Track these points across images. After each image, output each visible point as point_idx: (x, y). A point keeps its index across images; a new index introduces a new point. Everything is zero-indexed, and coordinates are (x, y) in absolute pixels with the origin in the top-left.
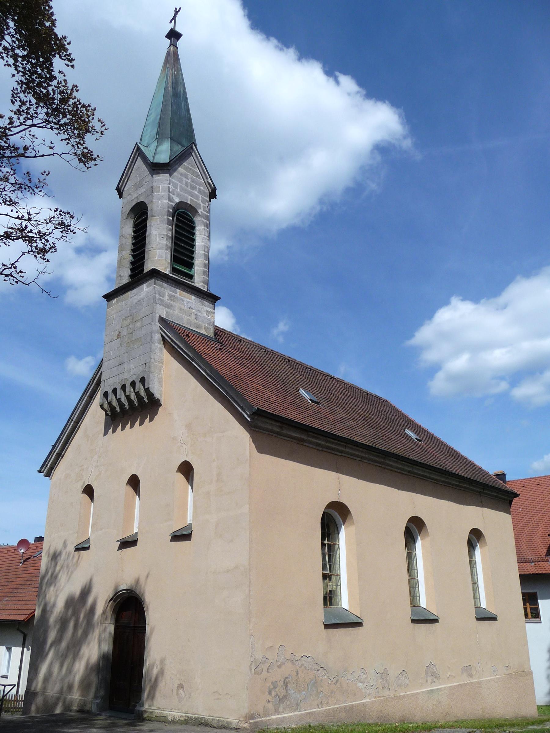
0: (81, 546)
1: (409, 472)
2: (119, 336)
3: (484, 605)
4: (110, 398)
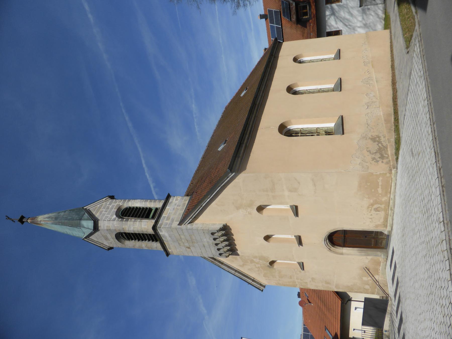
0: (302, 267)
1: (263, 93)
2: (189, 248)
3: (333, 56)
4: (222, 252)
